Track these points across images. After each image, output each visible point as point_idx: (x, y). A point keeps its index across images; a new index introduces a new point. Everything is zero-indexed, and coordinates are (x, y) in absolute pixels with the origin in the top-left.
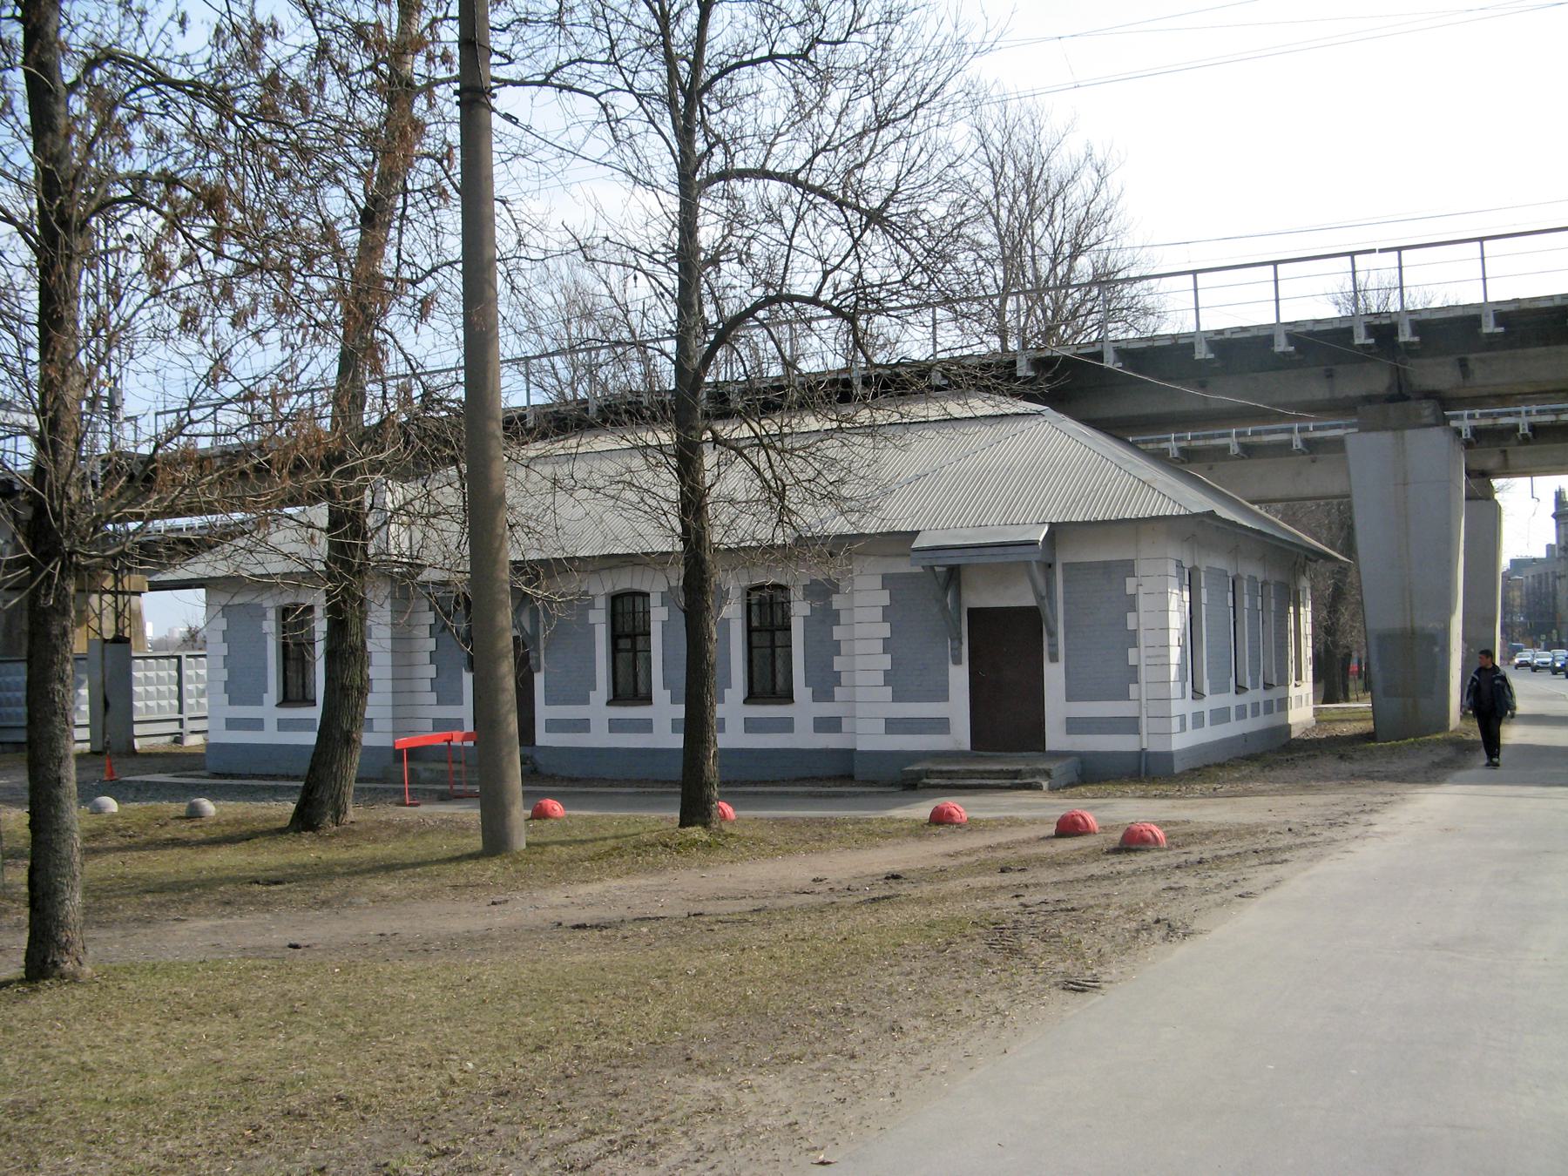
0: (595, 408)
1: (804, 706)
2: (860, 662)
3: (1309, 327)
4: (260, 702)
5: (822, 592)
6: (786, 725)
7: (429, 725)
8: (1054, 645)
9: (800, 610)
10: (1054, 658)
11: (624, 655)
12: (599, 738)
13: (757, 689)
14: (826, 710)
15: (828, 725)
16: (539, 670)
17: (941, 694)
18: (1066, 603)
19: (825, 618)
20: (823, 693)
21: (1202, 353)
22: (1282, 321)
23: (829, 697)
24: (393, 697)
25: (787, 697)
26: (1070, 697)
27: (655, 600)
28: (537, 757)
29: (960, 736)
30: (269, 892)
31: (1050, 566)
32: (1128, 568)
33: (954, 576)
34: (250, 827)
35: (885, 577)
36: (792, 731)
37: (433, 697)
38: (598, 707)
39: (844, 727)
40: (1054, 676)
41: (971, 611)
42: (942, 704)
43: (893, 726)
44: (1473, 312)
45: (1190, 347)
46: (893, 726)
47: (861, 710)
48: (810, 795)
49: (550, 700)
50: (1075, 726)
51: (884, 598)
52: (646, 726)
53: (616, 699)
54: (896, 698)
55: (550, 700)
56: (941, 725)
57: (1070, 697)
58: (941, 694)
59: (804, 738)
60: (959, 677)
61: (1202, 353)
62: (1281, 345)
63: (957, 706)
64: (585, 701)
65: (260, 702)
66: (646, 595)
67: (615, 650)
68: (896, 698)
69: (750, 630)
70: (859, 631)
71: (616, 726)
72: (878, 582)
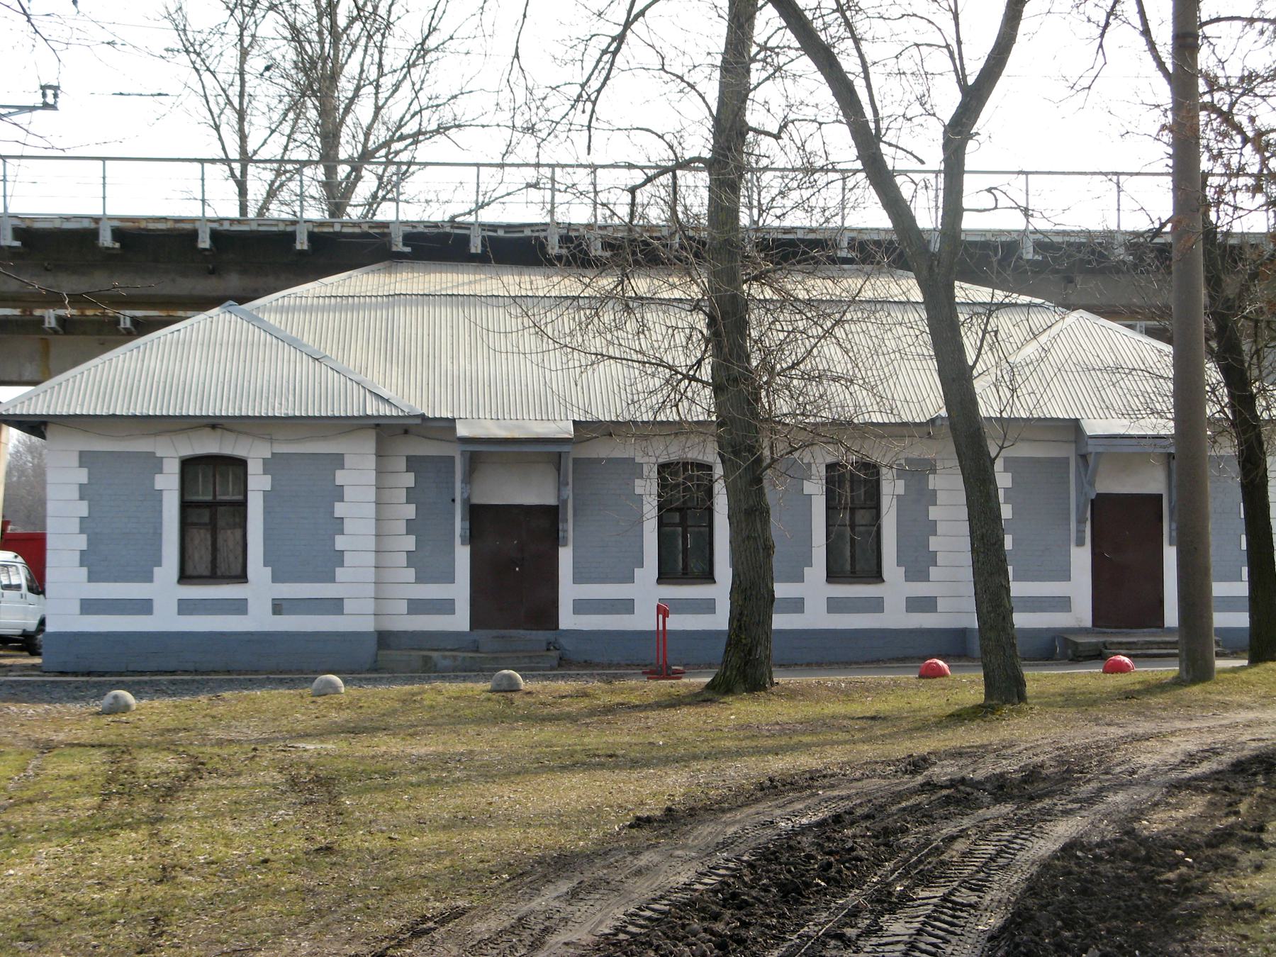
0: (556, 238)
3: (57, 224)
6: (876, 605)
7: (403, 607)
9: (891, 489)
12: (165, 620)
14: (920, 589)
16: (565, 545)
17: (1064, 574)
21: (1121, 254)
24: (376, 573)
25: (876, 576)
27: (254, 468)
29: (1081, 613)
32: (338, 461)
35: (82, 454)
37: (411, 572)
39: (78, 604)
40: (565, 556)
42: (330, 585)
43: (89, 606)
44: (86, 224)
45: (194, 235)
46: (89, 606)
48: (1030, 665)
49: (578, 578)
50: (581, 607)
52: (240, 607)
54: (92, 578)
55: (578, 578)
56: (1063, 604)
58: (1064, 574)
59: (895, 617)
60: (1081, 559)
61: (106, 240)
62: (106, 240)
63: (460, 590)
64: (630, 579)
66: (241, 464)
68: (92, 578)
71: (835, 606)
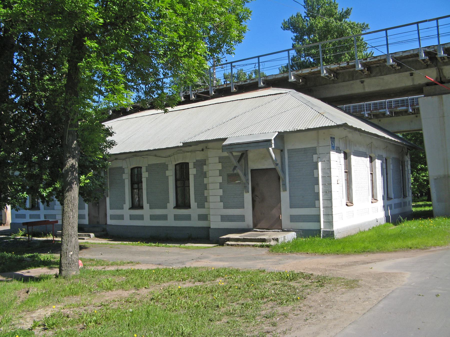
1: (146, 211)
2: (211, 192)
4: (166, 207)
5: (200, 164)
8: (284, 185)
9: (192, 171)
10: (285, 190)
11: (135, 191)
12: (127, 222)
13: (180, 202)
14: (202, 211)
15: (204, 217)
16: (108, 196)
18: (289, 166)
19: (202, 175)
20: (201, 205)
22: (440, 44)
23: (204, 207)
26: (292, 206)
28: (107, 228)
30: (183, 263)
31: (282, 151)
32: (314, 151)
33: (243, 156)
34: (148, 244)
36: (191, 220)
38: (126, 211)
40: (285, 196)
41: (252, 171)
43: (224, 218)
47: (212, 212)
51: (220, 166)
53: (177, 206)
54: (225, 207)
57: (292, 206)
59: (195, 223)
65: (166, 207)
67: (132, 189)
69: (176, 180)
70: (211, 180)
72: (217, 160)
